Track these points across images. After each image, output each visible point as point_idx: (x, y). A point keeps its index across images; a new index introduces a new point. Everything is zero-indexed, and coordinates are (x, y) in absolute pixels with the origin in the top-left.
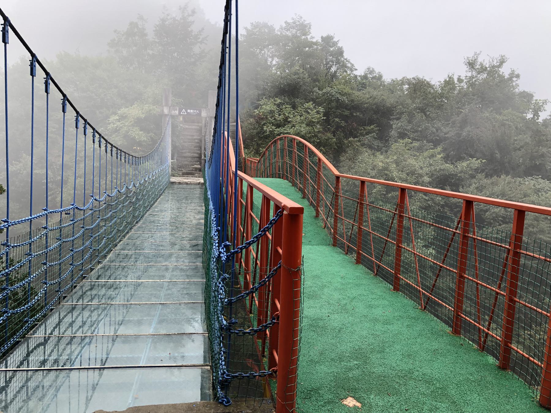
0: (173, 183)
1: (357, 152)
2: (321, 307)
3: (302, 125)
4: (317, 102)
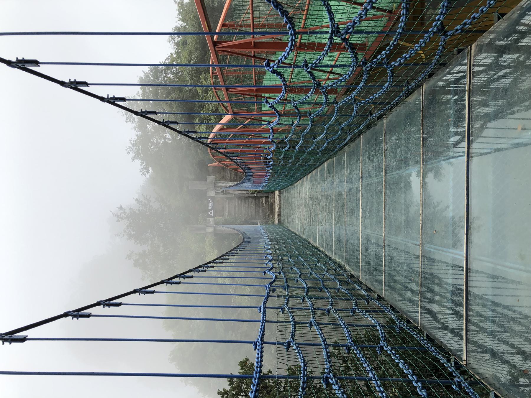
0: (279, 221)
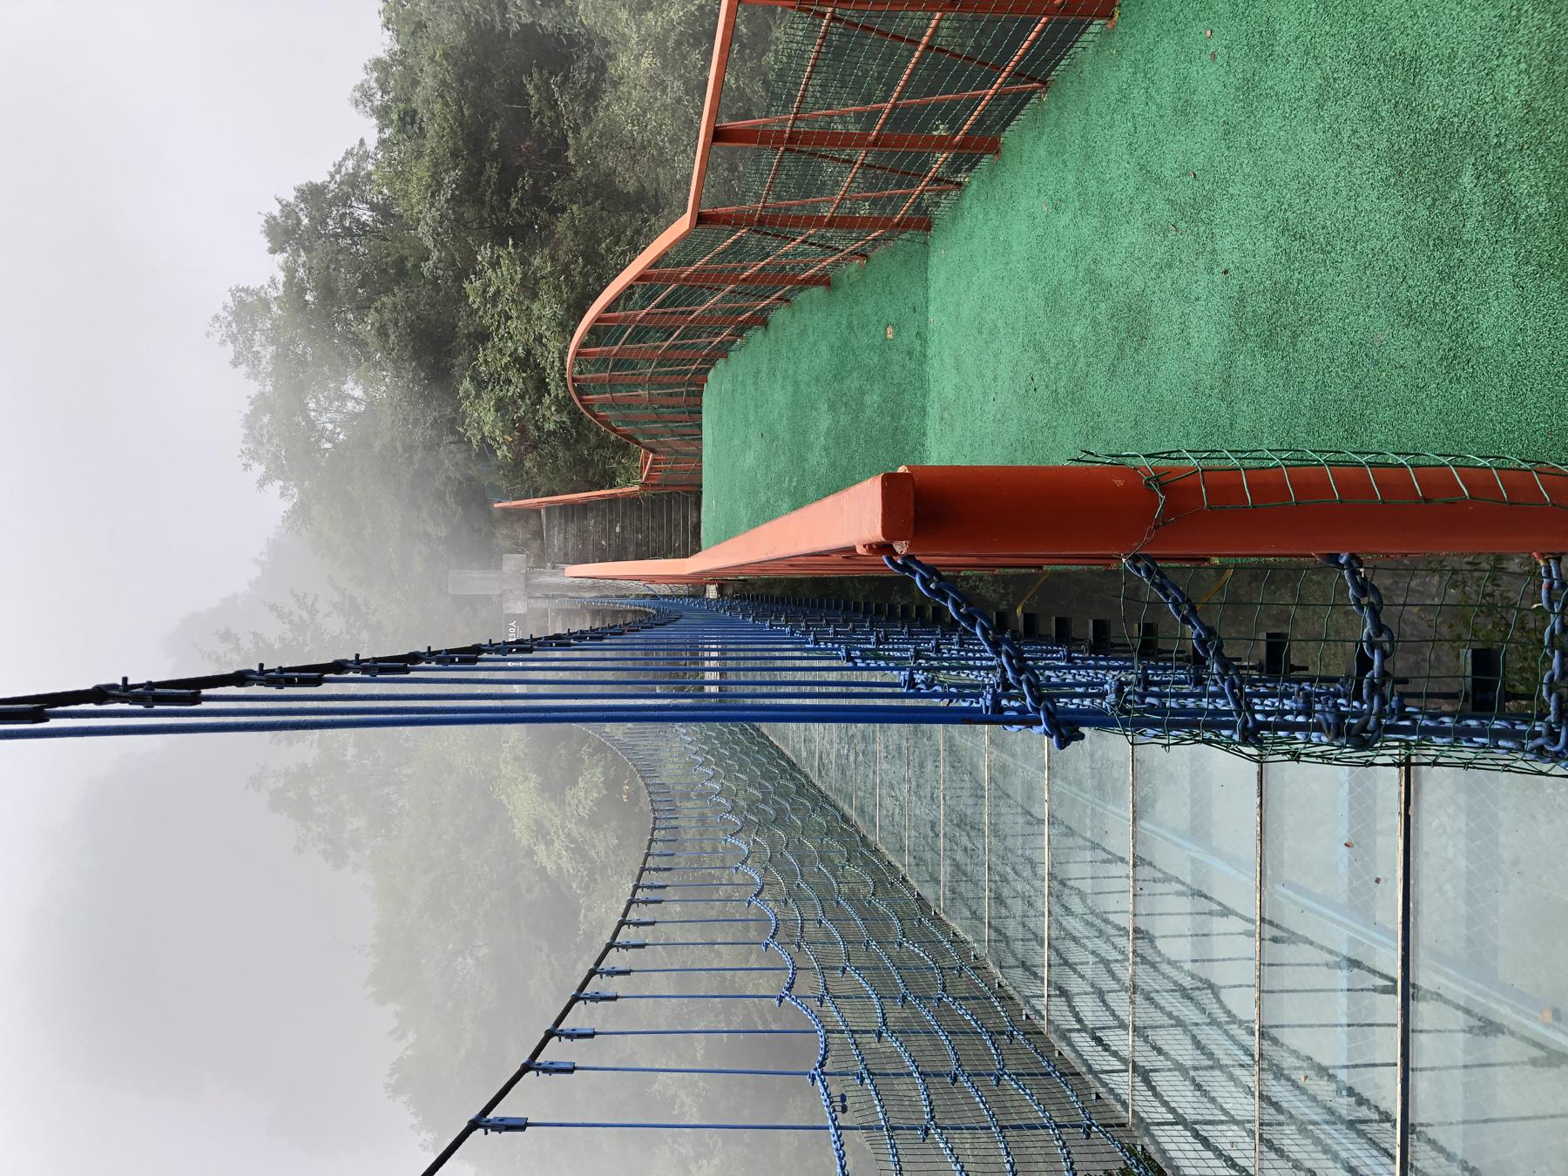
1: (611, 135)
2: (1183, 296)
3: (536, 313)
4: (464, 269)
